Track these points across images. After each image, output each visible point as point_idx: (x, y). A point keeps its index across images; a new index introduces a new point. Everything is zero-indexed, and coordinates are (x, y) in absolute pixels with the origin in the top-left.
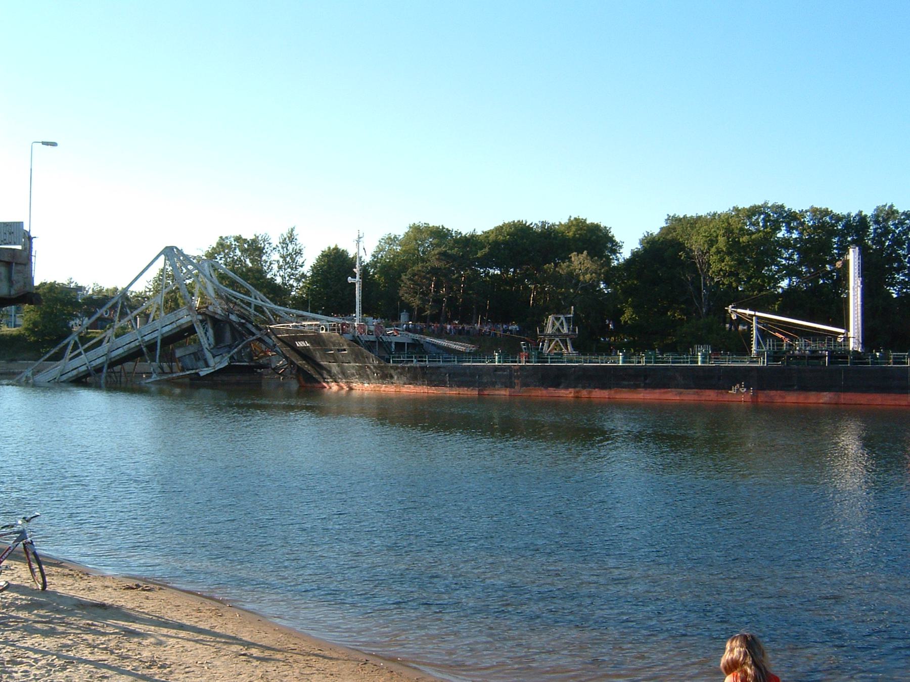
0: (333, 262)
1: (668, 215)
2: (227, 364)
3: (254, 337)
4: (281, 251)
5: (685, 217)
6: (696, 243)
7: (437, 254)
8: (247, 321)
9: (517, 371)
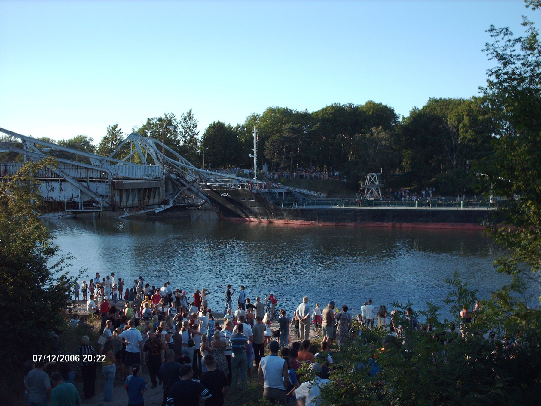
0: (218, 132)
1: (430, 98)
2: (172, 205)
3: (186, 188)
4: (183, 125)
5: (440, 99)
6: (451, 120)
7: (288, 129)
8: (180, 177)
9: (358, 212)
